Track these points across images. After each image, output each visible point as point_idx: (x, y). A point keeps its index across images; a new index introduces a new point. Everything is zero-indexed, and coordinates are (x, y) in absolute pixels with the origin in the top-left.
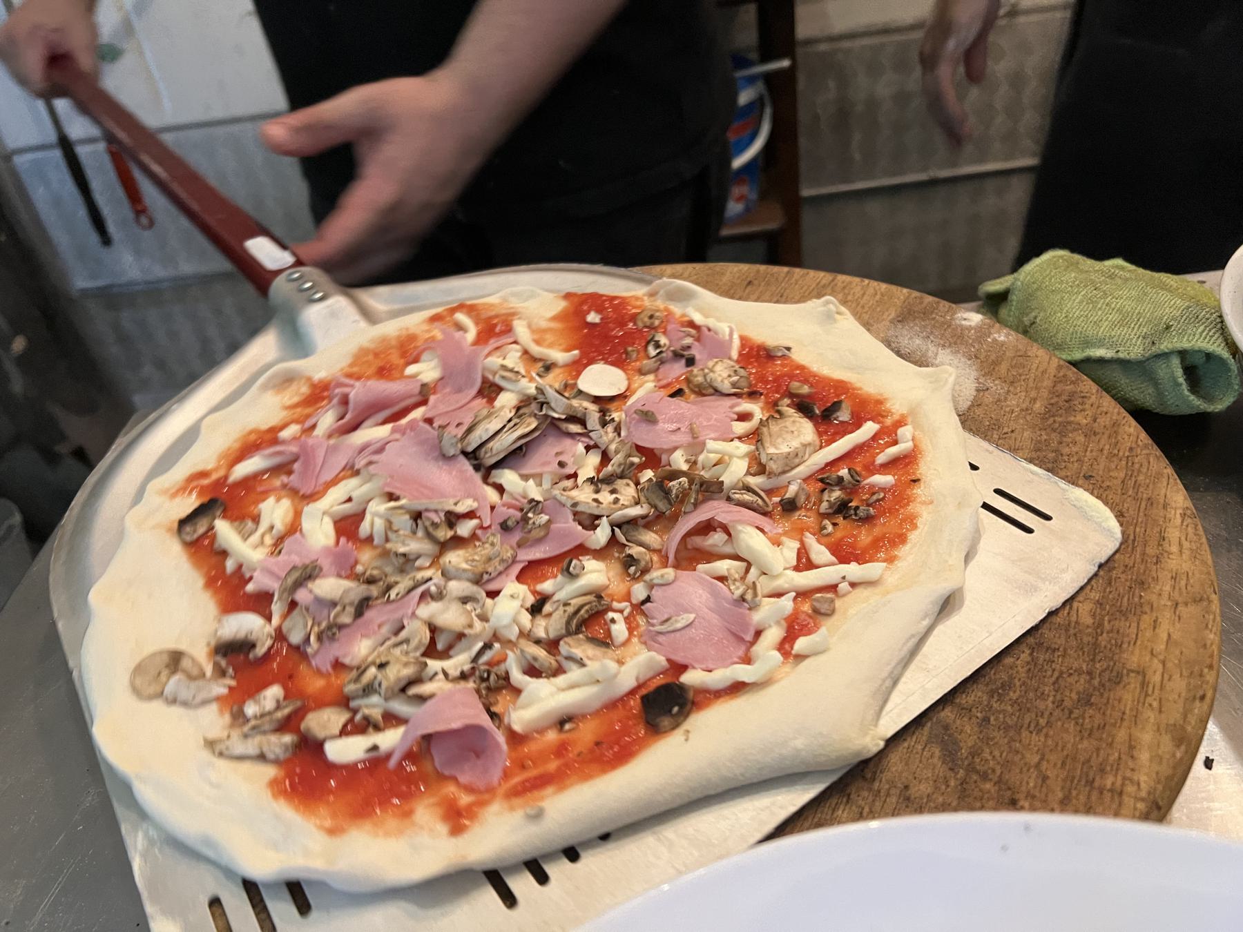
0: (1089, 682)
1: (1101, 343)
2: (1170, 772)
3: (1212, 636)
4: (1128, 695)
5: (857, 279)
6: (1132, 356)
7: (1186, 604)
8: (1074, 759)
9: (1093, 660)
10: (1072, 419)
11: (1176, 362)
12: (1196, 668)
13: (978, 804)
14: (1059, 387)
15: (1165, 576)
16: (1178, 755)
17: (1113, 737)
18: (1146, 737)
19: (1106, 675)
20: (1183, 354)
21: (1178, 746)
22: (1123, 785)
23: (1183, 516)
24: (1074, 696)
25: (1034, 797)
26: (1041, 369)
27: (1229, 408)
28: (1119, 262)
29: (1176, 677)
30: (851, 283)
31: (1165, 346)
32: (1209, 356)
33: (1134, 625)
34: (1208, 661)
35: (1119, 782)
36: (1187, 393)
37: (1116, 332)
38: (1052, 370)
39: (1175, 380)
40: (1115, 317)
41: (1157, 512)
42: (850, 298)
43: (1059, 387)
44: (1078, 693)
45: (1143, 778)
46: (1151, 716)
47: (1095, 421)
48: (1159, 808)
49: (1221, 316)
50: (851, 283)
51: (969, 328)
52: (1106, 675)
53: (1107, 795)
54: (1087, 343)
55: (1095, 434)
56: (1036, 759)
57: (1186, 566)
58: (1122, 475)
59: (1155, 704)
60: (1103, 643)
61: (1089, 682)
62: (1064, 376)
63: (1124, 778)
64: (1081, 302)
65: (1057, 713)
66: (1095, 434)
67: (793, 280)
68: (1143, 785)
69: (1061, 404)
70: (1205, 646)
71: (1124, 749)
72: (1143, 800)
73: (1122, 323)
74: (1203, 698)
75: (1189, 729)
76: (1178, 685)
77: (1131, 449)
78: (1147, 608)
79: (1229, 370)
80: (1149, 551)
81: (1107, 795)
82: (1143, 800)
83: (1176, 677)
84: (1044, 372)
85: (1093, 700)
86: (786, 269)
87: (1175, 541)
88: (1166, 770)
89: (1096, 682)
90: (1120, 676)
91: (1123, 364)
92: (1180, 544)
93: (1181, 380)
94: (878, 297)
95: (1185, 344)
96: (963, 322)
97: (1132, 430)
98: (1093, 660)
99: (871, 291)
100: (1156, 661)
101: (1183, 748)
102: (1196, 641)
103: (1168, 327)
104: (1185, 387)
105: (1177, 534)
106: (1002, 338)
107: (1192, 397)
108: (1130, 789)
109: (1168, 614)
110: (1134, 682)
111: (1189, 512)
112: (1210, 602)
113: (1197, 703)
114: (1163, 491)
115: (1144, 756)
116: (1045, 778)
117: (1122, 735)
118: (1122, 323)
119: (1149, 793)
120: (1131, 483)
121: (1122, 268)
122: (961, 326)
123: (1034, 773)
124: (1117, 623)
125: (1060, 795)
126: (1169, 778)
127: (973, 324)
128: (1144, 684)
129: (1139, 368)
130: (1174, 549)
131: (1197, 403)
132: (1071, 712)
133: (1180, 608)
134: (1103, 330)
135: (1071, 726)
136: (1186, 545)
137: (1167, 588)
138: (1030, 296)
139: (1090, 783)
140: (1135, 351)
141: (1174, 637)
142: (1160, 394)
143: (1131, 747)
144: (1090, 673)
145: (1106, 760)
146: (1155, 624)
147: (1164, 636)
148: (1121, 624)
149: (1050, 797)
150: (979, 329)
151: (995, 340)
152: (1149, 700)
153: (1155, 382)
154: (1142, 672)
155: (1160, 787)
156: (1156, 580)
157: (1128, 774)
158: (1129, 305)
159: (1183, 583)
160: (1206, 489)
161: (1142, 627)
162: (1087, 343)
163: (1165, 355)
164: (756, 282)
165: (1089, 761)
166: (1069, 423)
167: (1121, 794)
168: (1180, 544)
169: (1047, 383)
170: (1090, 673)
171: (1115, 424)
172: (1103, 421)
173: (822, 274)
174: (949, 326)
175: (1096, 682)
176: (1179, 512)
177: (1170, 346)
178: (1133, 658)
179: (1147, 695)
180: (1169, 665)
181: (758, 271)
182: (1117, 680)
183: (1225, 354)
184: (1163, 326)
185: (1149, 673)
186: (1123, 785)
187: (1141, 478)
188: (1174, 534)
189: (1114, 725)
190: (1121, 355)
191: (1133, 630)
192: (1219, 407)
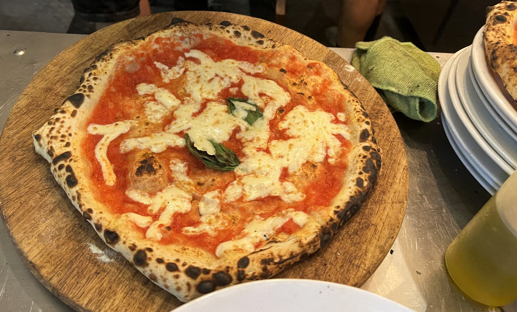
0: (359, 226)
1: (393, 85)
2: (376, 262)
3: (401, 216)
4: (369, 233)
5: (311, 40)
6: (404, 94)
7: (396, 203)
8: (347, 253)
9: (362, 218)
10: (376, 121)
11: (418, 101)
12: (393, 227)
13: (245, 59)
14: (375, 107)
15: (392, 191)
16: (380, 256)
17: (361, 247)
18: (372, 249)
19: (365, 225)
20: (420, 98)
21: (381, 254)
22: (361, 264)
23: (404, 169)
24: (353, 230)
25: (332, 264)
26: (370, 97)
27: (431, 122)
28: (410, 44)
29: (386, 229)
30: (309, 41)
31: (415, 94)
32: (429, 102)
33: (378, 207)
34: (398, 225)
35: (360, 263)
36: (418, 114)
37: (400, 82)
38: (374, 99)
39: (415, 108)
40: (401, 76)
41: (396, 165)
42: (307, 48)
43: (375, 107)
44: (354, 229)
45: (367, 263)
46: (375, 241)
47: (384, 124)
48: (370, 273)
49: (437, 86)
50: (309, 41)
51: (349, 73)
52: (365, 225)
53: (355, 266)
54: (389, 84)
55: (383, 129)
56: (335, 251)
57: (400, 188)
58: (388, 149)
59: (377, 238)
60: (366, 213)
61: (359, 226)
62: (378, 102)
63: (361, 262)
64: (391, 66)
65: (346, 235)
66: (383, 129)
67: (287, 35)
68: (367, 265)
69: (374, 114)
70: (398, 220)
71: (364, 252)
72: (365, 270)
73: (403, 79)
74: (393, 238)
75: (386, 248)
76: (386, 232)
77: (393, 138)
78: (383, 202)
79: (434, 108)
80: (390, 181)
81: (355, 266)
82: (365, 270)
83: (386, 229)
84: (371, 99)
85: (358, 232)
86: (285, 28)
87: (399, 178)
88: (375, 261)
89: (361, 227)
90: (369, 225)
91: (400, 96)
92: (400, 180)
93: (417, 108)
94: (318, 50)
95: (422, 96)
96: (347, 70)
97: (396, 130)
98: (362, 218)
99: (315, 47)
100: (381, 222)
101: (382, 254)
102: (396, 217)
103: (418, 86)
104: (418, 111)
105: (400, 176)
106: (360, 80)
107: (420, 116)
108: (362, 266)
109: (389, 205)
110: (372, 228)
111: (406, 168)
112: (404, 203)
113: (390, 240)
114: (400, 158)
115: (369, 255)
116: (337, 258)
117: (364, 247)
118: (403, 79)
119: (368, 268)
120: (390, 152)
121: (410, 47)
122: (346, 71)
123: (334, 256)
124: (372, 206)
125: (341, 264)
126: (375, 264)
127: (350, 71)
128: (376, 230)
129: (406, 99)
130: (398, 181)
131: (421, 118)
132: (350, 236)
133: (394, 204)
134: (395, 81)
135: (349, 241)
136: (402, 180)
137: (392, 196)
138: (374, 58)
139: (351, 262)
140: (405, 92)
141: (389, 214)
142: (409, 110)
143: (366, 251)
144: (359, 223)
145: (357, 255)
146: (385, 209)
147: (386, 213)
148: (374, 206)
149: (337, 265)
150: (352, 74)
151: (357, 80)
152: (376, 235)
153: (409, 105)
154: (376, 226)
155: (372, 266)
156: (389, 192)
157: (363, 260)
158: (407, 72)
159: (397, 195)
160: (417, 148)
161: (380, 209)
162: (389, 84)
163: (415, 97)
164: (272, 32)
165: (352, 254)
166: (375, 123)
167: (359, 267)
168: (400, 180)
169: (371, 104)
170: (359, 223)
171: (391, 127)
172: (387, 124)
173: (298, 34)
174: (342, 70)
175: (361, 227)
176: (403, 167)
177: (417, 94)
178: (374, 220)
179: (376, 234)
180: (385, 224)
181: (274, 27)
182: (368, 227)
183: (434, 102)
184: (416, 85)
185: (378, 226)
186: (361, 264)
187: (394, 151)
188: (399, 176)
189: (363, 243)
190: (400, 93)
191: (377, 209)
192: (428, 121)
